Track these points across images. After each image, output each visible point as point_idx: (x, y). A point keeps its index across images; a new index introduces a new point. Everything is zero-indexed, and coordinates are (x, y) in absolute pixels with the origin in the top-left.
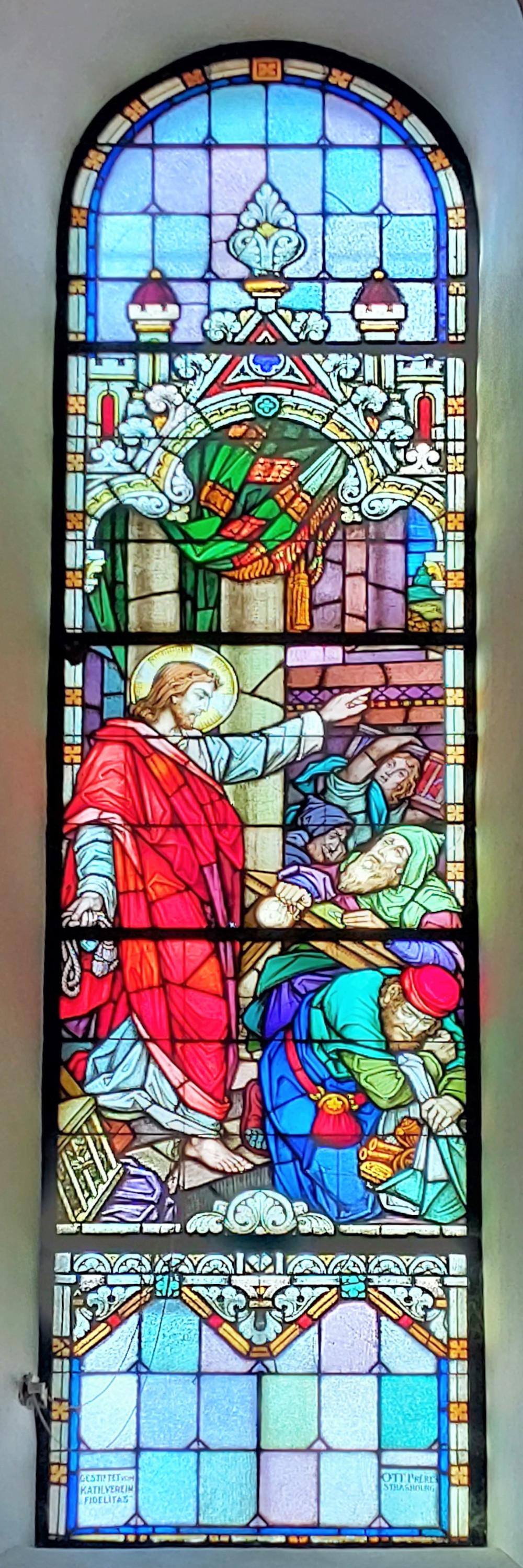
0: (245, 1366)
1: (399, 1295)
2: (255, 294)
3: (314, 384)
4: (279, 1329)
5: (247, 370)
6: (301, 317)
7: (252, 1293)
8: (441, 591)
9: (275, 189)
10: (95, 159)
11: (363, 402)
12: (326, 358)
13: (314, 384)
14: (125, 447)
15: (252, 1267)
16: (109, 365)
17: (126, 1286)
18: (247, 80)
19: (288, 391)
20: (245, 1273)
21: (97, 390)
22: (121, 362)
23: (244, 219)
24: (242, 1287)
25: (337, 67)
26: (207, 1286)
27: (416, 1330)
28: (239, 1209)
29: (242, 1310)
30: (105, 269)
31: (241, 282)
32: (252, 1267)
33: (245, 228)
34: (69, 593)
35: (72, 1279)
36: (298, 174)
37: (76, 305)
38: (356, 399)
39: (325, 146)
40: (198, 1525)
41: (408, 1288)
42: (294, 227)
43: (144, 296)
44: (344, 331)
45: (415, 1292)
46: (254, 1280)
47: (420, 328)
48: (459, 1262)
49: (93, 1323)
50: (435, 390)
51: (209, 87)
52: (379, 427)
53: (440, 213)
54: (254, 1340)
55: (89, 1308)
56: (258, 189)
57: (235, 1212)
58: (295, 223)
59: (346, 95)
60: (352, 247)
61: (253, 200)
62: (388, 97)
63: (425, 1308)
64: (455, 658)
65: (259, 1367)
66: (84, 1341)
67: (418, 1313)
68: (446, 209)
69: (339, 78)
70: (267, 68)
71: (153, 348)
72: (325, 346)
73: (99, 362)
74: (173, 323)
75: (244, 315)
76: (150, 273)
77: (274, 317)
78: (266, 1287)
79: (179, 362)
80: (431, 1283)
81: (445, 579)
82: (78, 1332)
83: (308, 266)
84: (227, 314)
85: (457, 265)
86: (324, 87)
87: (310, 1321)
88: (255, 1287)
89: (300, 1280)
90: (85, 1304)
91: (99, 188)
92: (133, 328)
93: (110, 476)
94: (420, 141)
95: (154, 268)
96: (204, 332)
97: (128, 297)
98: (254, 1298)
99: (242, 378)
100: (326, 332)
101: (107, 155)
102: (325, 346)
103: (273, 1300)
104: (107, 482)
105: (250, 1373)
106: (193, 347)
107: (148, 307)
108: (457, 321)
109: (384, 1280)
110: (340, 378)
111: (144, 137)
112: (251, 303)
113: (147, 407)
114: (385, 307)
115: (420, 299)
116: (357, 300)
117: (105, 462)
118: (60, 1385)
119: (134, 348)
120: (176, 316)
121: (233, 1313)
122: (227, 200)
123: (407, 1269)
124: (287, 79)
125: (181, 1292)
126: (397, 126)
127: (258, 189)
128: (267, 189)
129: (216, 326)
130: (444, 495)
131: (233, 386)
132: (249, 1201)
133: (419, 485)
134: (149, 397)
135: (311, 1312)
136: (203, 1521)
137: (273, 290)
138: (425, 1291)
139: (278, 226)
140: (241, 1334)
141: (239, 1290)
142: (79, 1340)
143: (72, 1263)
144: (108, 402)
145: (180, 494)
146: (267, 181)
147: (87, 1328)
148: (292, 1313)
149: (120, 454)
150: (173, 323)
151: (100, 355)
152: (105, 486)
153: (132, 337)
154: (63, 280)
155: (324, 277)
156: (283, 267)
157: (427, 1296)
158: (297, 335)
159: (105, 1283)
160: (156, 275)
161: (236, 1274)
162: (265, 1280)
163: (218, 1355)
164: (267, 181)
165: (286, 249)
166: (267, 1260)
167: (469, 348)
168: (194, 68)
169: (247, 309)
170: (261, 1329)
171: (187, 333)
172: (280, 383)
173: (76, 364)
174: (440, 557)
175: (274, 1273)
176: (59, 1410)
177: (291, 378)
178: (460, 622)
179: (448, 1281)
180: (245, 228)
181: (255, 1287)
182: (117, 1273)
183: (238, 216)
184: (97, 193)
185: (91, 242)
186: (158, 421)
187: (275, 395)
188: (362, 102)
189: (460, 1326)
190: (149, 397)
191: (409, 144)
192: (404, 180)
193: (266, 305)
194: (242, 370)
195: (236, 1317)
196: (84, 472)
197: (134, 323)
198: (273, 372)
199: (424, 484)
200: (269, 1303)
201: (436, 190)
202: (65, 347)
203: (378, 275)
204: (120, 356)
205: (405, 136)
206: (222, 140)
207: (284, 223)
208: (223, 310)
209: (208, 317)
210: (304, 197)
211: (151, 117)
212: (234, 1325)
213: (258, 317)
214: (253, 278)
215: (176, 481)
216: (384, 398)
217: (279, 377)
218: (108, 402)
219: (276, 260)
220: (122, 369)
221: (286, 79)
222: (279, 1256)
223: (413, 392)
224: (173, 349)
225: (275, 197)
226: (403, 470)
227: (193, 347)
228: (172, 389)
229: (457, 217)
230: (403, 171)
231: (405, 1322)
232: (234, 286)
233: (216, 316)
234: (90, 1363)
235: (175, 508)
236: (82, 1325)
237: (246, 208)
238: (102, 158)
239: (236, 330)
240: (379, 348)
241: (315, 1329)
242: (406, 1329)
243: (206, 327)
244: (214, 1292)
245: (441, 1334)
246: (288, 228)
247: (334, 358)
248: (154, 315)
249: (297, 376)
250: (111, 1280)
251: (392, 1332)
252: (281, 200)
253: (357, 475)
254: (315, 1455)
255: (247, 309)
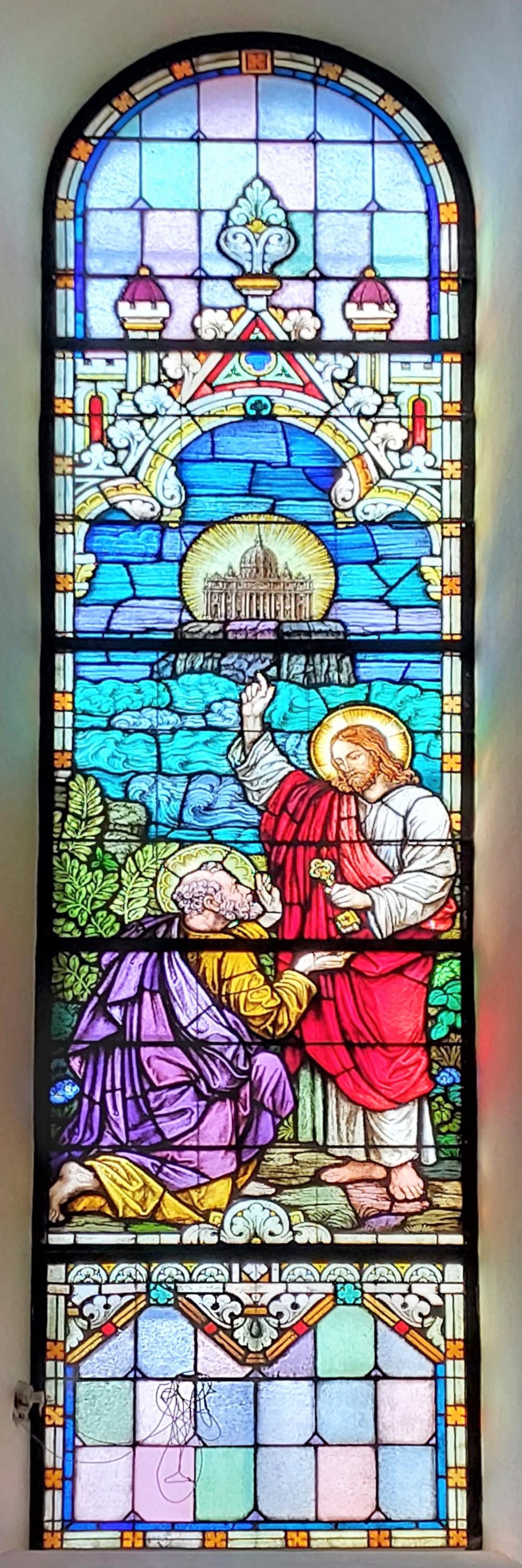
0: (243, 1372)
1: (396, 1301)
2: (245, 292)
3: (308, 387)
4: (275, 1335)
5: (239, 370)
6: (293, 315)
7: (247, 1300)
8: (436, 596)
9: (266, 184)
10: (82, 149)
11: (355, 406)
12: (317, 359)
13: (308, 387)
14: (116, 451)
15: (248, 1275)
16: (97, 364)
17: (122, 1295)
18: (238, 71)
19: (279, 392)
20: (241, 1281)
21: (84, 393)
22: (110, 362)
23: (233, 215)
24: (237, 1294)
25: (326, 60)
26: (202, 1294)
27: (413, 1336)
28: (235, 1220)
29: (237, 1317)
30: (93, 265)
31: (231, 279)
32: (248, 1275)
33: (235, 225)
34: (59, 597)
35: (66, 1289)
36: (290, 172)
37: (65, 298)
38: (350, 402)
39: (314, 140)
40: (195, 1521)
41: (404, 1295)
42: (284, 224)
43: (133, 294)
44: (336, 331)
45: (412, 1300)
46: (249, 1287)
47: (412, 326)
48: (455, 1271)
49: (88, 1333)
50: (429, 393)
51: (196, 79)
52: (373, 430)
53: (431, 212)
54: (250, 1348)
55: (84, 1318)
56: (250, 184)
57: (232, 1224)
58: (287, 220)
59: (336, 86)
60: (341, 244)
61: (244, 196)
62: (380, 91)
63: (232, 1316)
64: (453, 666)
65: (256, 1374)
66: (77, 1352)
67: (416, 1321)
68: (438, 205)
69: (331, 70)
70: (252, 57)
71: (143, 346)
72: (318, 346)
73: (87, 361)
74: (164, 321)
75: (235, 314)
76: (139, 268)
77: (265, 316)
78: (262, 1294)
79: (166, 363)
80: (428, 1291)
81: (442, 585)
82: (72, 1342)
83: (300, 264)
84: (219, 312)
85: (449, 259)
86: (315, 80)
87: (306, 1328)
88: (250, 1295)
89: (293, 1288)
90: (81, 1316)
91: (85, 182)
92: (122, 325)
93: (97, 480)
94: (415, 138)
95: (142, 265)
96: (195, 330)
97: (116, 294)
98: (248, 1306)
99: (234, 378)
100: (319, 331)
101: (95, 146)
102: (318, 346)
103: (267, 1307)
104: (98, 485)
105: (246, 1378)
106: (180, 346)
107: (139, 305)
108: (449, 328)
109: (380, 1288)
110: (334, 380)
111: (129, 130)
112: (239, 300)
113: (137, 406)
114: (148, 305)
115: (413, 297)
116: (122, 298)
117: (94, 465)
118: (54, 1391)
119: (124, 345)
120: (167, 315)
121: (228, 1320)
122: (218, 196)
123: (320, 1274)
124: (276, 72)
125: (177, 1301)
126: (388, 120)
127: (250, 184)
128: (258, 184)
129: (213, 325)
130: (440, 501)
131: (223, 387)
132: (246, 1213)
133: (414, 489)
134: (139, 398)
135: (305, 1320)
136: (200, 1516)
137: (264, 288)
138: (421, 1298)
139: (268, 224)
140: (430, 1341)
141: (234, 1298)
142: (72, 1349)
143: (67, 1274)
144: (96, 400)
145: (172, 497)
146: (258, 176)
147: (81, 1338)
148: (289, 1318)
149: (110, 457)
150: (164, 321)
151: (89, 355)
152: (96, 490)
153: (120, 334)
154: (50, 276)
155: (317, 277)
156: (281, 262)
157: (423, 1303)
158: (289, 334)
159: (100, 1293)
160: (144, 272)
161: (230, 1281)
162: (263, 1288)
163: (214, 1360)
164: (258, 176)
165: (277, 249)
166: (263, 1268)
167: (465, 348)
168: (182, 59)
169: (238, 307)
170: (260, 1334)
171: (178, 330)
172: (271, 384)
173: (64, 365)
174: (436, 561)
175: (270, 1281)
176: (55, 1416)
177: (283, 379)
178: (457, 629)
179: (444, 1288)
180: (235, 225)
181: (250, 1295)
182: (114, 1282)
183: (228, 212)
184: (350, 93)
185: (359, 98)
186: (148, 424)
187: (267, 397)
188: (355, 96)
189: (457, 1326)
190: (139, 398)
191: (402, 139)
192: (396, 178)
193: (258, 304)
194: (234, 369)
195: (232, 1324)
196: (73, 475)
197: (122, 322)
198: (266, 371)
199: (419, 488)
200: (263, 1311)
201: (429, 188)
202: (51, 345)
203: (370, 273)
204: (110, 355)
205: (399, 131)
206: (209, 135)
207: (273, 220)
208: (215, 309)
209: (200, 313)
210: (297, 197)
211: (138, 108)
212: (231, 1332)
213: (250, 315)
214: (246, 275)
215: (167, 484)
216: (379, 401)
217: (268, 378)
218: (96, 400)
219: (266, 258)
220: (110, 369)
221: (276, 71)
222: (275, 1266)
223: (407, 395)
224: (164, 346)
225: (267, 192)
226: (397, 475)
227: (180, 346)
228: (162, 391)
229: (449, 213)
230: (393, 165)
231: (401, 1329)
232: (226, 285)
233: (207, 313)
234: (84, 1371)
235: (166, 511)
236: (77, 1334)
237: (236, 204)
238: (90, 148)
239: (226, 329)
240: (372, 348)
241: (311, 1334)
242: (403, 1336)
243: (197, 324)
244: (210, 1300)
245: (439, 1340)
246: (279, 225)
247: (326, 357)
248: (143, 315)
249: (288, 376)
250: (106, 1289)
251: (390, 1339)
252: (273, 196)
253: (351, 479)
254: (312, 1449)
255: (238, 307)
